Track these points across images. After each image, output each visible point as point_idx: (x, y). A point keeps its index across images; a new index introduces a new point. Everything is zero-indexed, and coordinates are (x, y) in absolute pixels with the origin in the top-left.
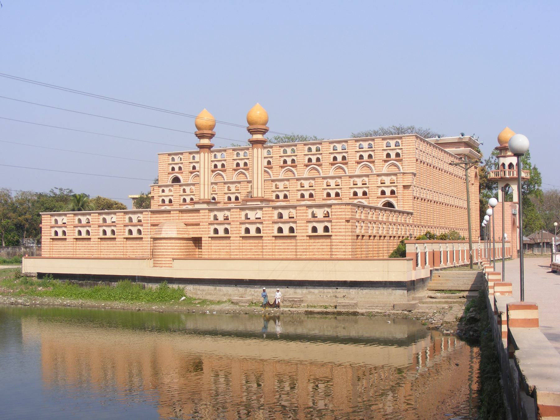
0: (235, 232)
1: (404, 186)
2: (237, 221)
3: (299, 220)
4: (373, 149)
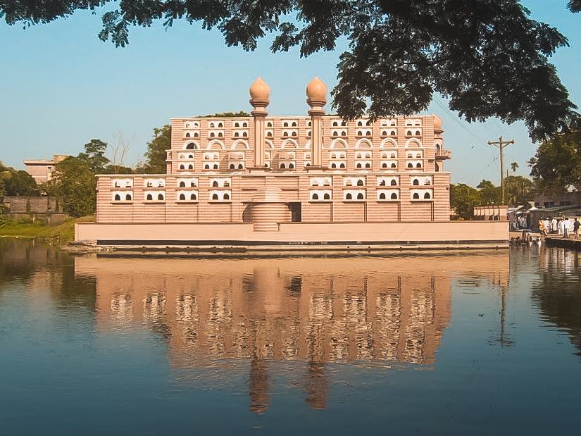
4: (223, 128)
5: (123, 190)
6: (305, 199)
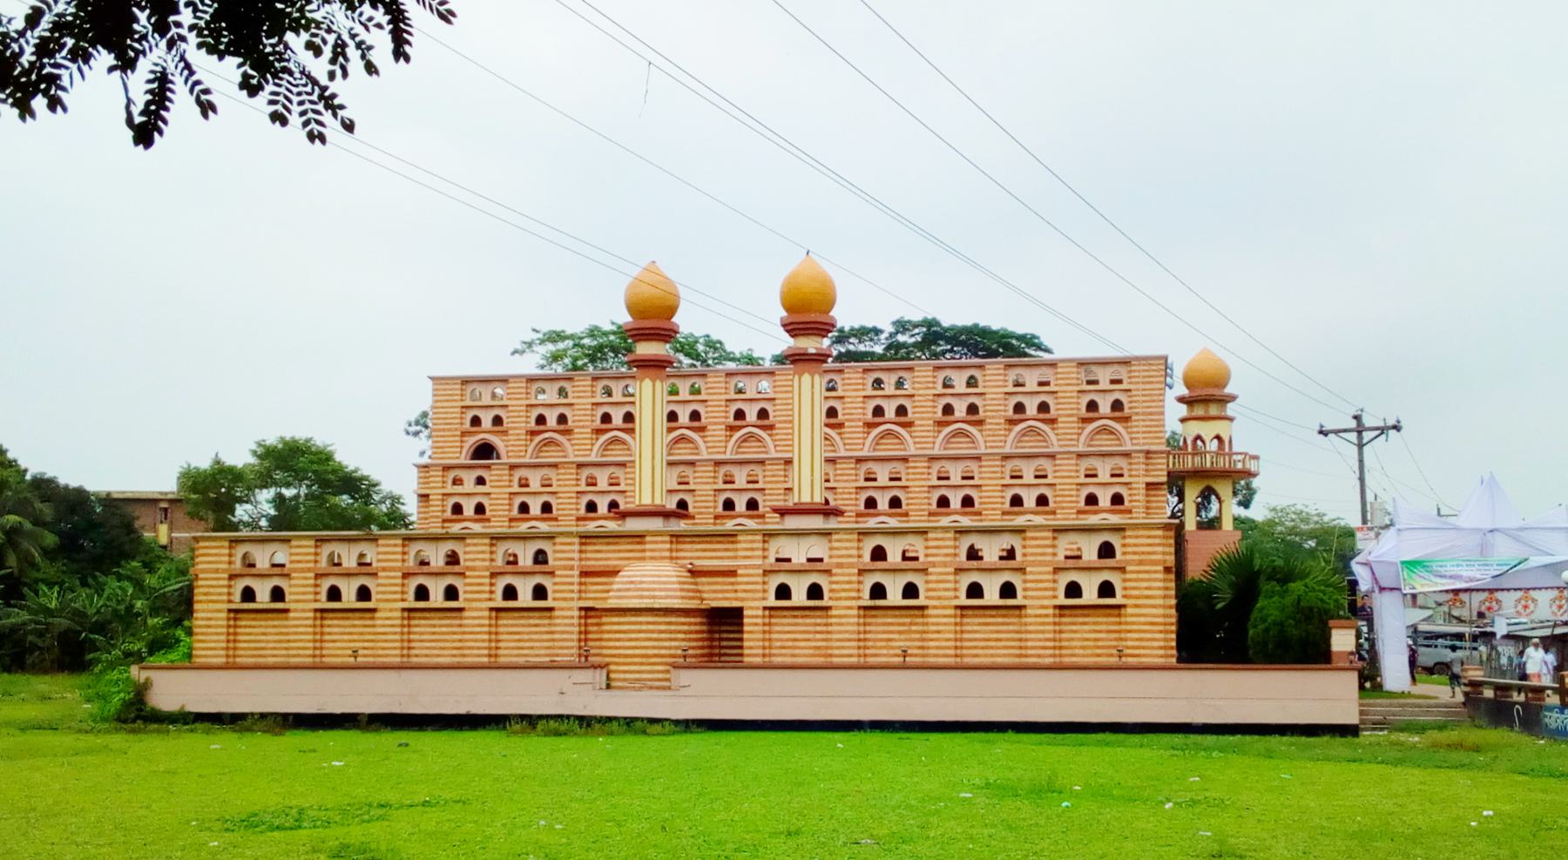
0: (843, 594)
1: (1148, 484)
2: (850, 565)
3: (1033, 564)
4: (839, 393)
5: (991, 570)
6: (753, 597)
